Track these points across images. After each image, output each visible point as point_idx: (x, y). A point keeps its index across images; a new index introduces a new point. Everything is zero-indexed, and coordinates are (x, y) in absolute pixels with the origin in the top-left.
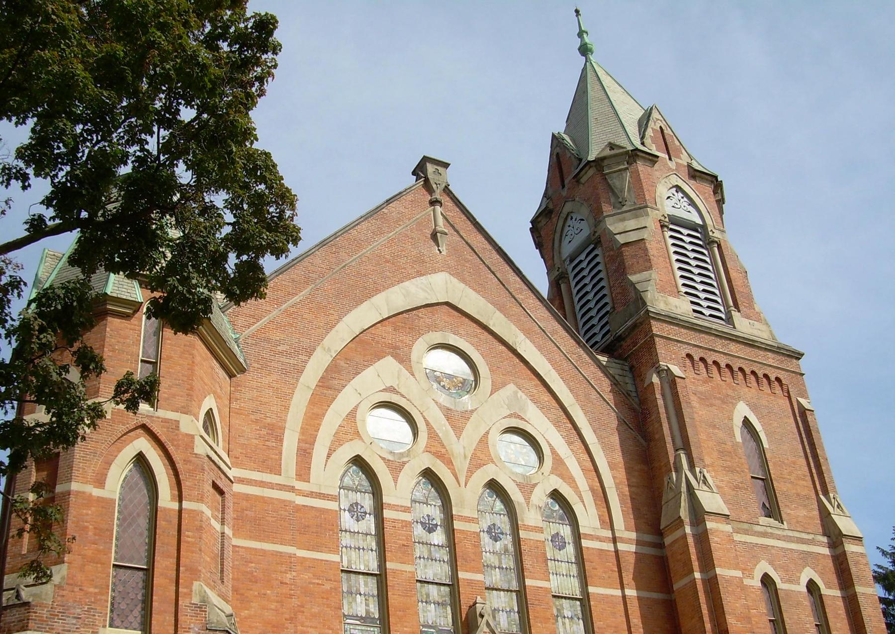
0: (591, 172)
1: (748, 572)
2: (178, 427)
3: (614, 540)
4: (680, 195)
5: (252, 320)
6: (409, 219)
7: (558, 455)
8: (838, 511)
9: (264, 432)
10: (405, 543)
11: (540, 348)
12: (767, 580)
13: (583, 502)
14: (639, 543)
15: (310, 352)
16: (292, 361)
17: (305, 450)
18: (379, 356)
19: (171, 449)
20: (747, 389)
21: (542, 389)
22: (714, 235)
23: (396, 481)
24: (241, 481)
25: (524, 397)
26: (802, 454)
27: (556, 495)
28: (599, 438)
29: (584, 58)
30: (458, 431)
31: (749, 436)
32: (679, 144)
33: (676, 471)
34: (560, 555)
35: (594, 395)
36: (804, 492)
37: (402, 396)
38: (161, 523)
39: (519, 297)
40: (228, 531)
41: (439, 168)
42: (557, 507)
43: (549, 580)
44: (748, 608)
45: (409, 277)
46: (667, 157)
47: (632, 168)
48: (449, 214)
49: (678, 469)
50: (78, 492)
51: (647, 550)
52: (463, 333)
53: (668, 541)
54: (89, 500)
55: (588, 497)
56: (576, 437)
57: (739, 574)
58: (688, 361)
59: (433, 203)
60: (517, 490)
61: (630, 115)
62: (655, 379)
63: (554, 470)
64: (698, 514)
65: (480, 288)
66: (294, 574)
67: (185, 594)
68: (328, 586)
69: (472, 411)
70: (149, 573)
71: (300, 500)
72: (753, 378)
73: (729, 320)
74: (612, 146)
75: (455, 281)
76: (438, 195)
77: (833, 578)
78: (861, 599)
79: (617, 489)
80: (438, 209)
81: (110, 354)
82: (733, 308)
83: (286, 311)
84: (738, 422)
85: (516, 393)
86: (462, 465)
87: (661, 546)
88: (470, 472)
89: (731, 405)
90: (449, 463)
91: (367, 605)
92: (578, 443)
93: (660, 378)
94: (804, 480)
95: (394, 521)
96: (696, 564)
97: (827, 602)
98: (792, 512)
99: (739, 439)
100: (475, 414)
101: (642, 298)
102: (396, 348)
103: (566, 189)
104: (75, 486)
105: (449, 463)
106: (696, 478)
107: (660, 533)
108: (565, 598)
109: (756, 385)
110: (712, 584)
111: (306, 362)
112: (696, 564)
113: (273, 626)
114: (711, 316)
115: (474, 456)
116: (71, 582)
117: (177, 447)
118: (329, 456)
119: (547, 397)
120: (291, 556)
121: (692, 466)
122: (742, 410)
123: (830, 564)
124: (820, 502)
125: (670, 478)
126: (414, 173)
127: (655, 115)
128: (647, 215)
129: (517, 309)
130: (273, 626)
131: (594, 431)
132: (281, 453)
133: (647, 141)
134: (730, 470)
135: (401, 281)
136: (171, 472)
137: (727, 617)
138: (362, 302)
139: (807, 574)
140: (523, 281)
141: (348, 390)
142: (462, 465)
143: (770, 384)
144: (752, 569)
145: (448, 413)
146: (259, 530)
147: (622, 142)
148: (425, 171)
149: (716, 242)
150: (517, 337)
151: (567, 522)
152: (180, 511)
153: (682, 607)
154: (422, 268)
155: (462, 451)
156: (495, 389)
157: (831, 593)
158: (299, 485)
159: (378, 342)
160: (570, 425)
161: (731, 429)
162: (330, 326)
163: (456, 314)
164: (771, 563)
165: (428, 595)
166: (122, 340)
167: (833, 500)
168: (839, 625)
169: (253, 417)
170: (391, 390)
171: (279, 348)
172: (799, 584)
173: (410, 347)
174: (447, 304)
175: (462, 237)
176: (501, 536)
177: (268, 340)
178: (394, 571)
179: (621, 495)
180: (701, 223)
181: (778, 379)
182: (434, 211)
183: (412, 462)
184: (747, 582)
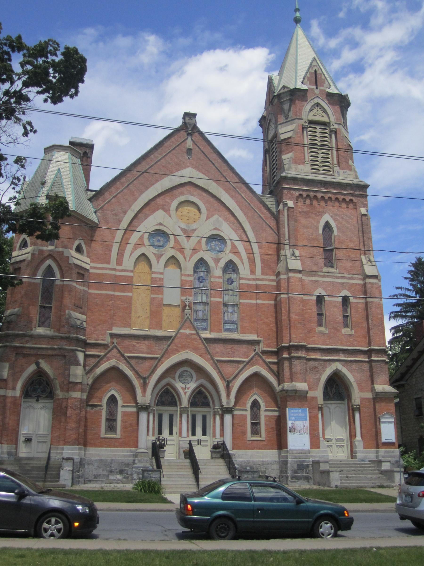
11: (232, 197)
15: (125, 213)
35: (256, 215)
37: (165, 226)
55: (246, 262)
60: (212, 261)
69: (196, 229)
71: (118, 273)
88: (192, 256)
100: (197, 231)
111: (124, 217)
114: (324, 170)
118: (130, 255)
119: (232, 219)
120: (112, 295)
122: (327, 217)
131: (254, 232)
138: (150, 187)
142: (188, 253)
154: (180, 166)
156: (208, 218)
158: (118, 267)
161: (318, 228)
164: (324, 289)
170: (160, 224)
173: (170, 204)
175: (200, 149)
176: (204, 281)
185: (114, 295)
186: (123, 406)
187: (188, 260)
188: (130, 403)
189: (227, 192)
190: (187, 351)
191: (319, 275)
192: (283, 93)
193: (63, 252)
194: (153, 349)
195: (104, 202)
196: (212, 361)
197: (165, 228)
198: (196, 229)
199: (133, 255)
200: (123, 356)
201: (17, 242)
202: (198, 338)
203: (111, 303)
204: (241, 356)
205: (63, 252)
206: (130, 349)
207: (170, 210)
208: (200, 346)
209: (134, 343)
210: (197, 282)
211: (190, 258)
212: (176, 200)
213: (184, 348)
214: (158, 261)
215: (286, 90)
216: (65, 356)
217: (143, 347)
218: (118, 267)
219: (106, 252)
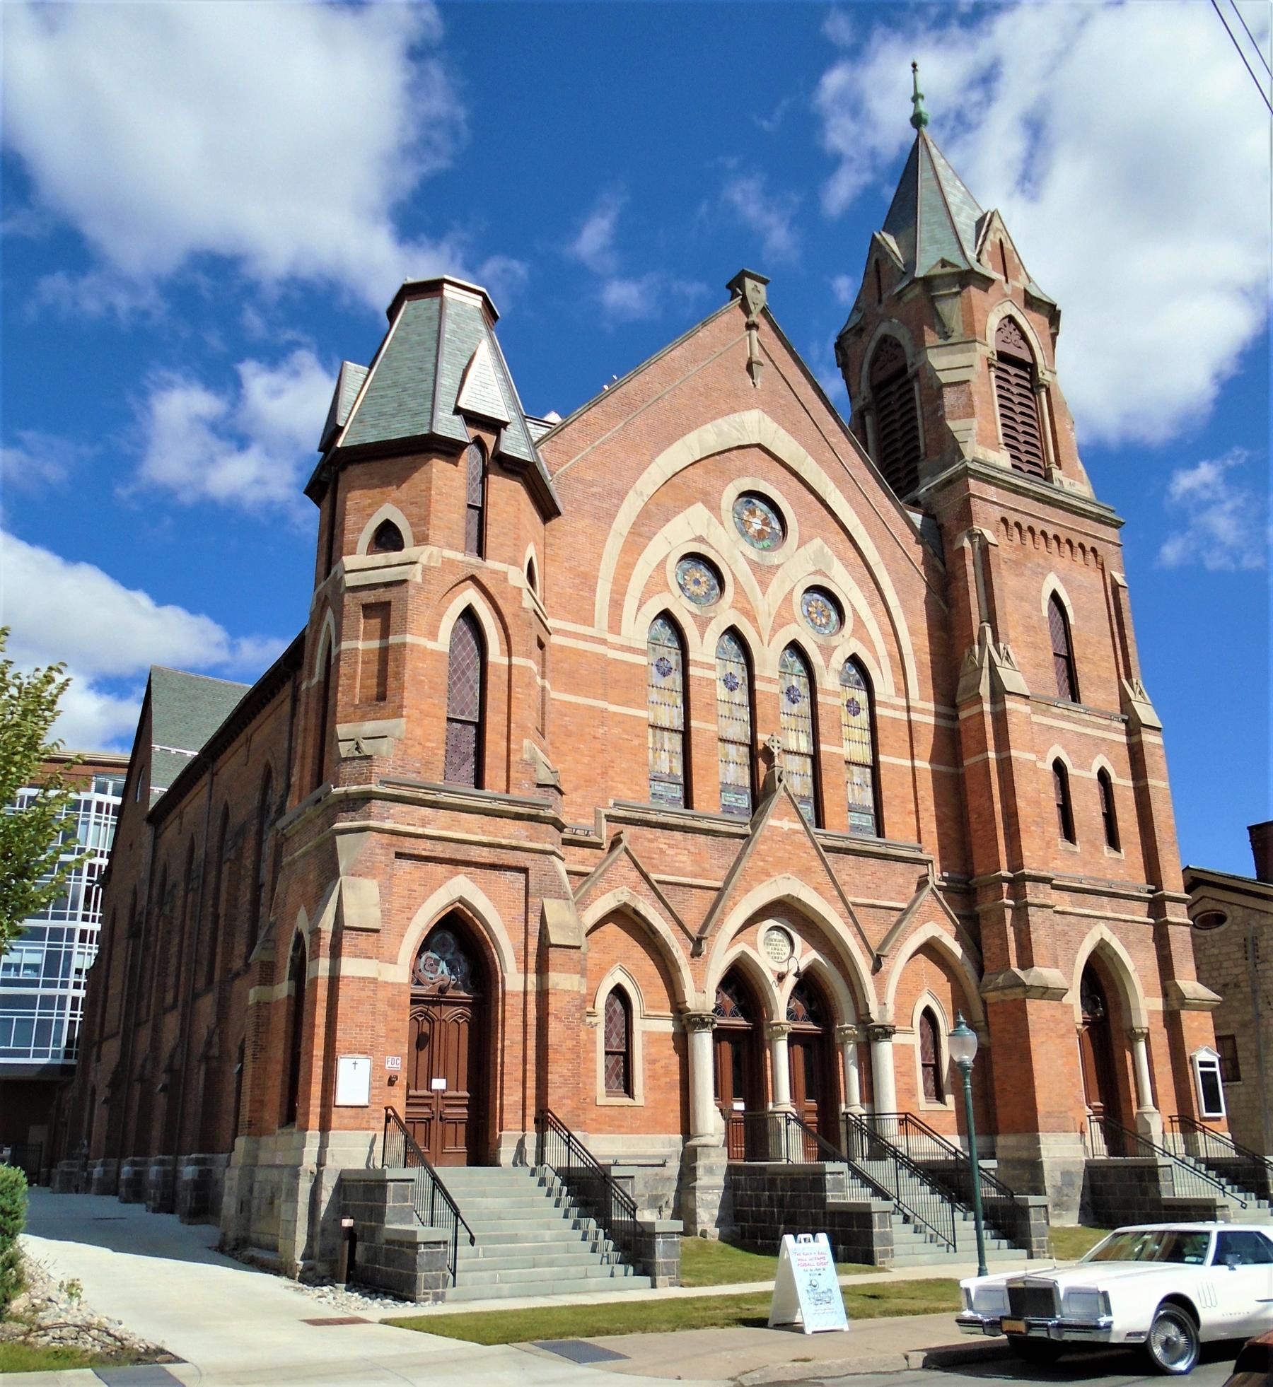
0: (917, 290)
1: (1042, 756)
2: (506, 579)
3: (908, 709)
4: (1013, 326)
5: (566, 458)
6: (724, 345)
7: (859, 617)
8: (1139, 698)
9: (577, 581)
10: (709, 701)
11: (849, 499)
12: (1059, 767)
13: (880, 668)
14: (937, 715)
15: (622, 496)
16: (604, 505)
17: (616, 602)
18: (690, 503)
19: (500, 602)
20: (1060, 559)
21: (849, 544)
22: (1044, 377)
23: (702, 637)
24: (558, 631)
25: (830, 552)
26: (1109, 633)
27: (854, 660)
28: (902, 601)
29: (915, 130)
30: (764, 585)
31: (1056, 609)
32: (1012, 248)
33: (979, 644)
34: (855, 721)
36: (1105, 675)
38: (491, 678)
39: (832, 440)
40: (548, 686)
41: (758, 284)
42: (854, 671)
43: (842, 746)
44: (1039, 792)
45: (722, 414)
46: (1003, 278)
47: (965, 293)
48: (765, 341)
49: (982, 643)
50: (413, 645)
51: (943, 723)
52: (773, 478)
53: (963, 715)
54: (425, 652)
56: (879, 599)
57: (1032, 757)
58: (1002, 527)
59: (751, 326)
60: (817, 651)
61: (965, 222)
62: (966, 543)
63: (854, 633)
64: (998, 692)
65: (793, 431)
66: (606, 728)
67: (517, 750)
68: (636, 742)
69: (778, 566)
70: (480, 727)
72: (1067, 547)
73: (1048, 477)
74: (944, 263)
75: (768, 419)
76: (756, 317)
77: (1127, 769)
78: (1152, 792)
79: (915, 656)
80: (754, 333)
81: (438, 498)
82: (1054, 465)
83: (598, 447)
84: (1046, 595)
85: (822, 548)
86: (766, 622)
87: (955, 718)
88: (774, 631)
89: (1040, 576)
90: (753, 619)
91: (671, 761)
92: (881, 605)
93: (972, 543)
94: (1106, 661)
95: (700, 678)
96: (991, 743)
97: (1116, 791)
98: (1091, 695)
99: (1045, 613)
101: (959, 450)
102: (707, 494)
103: (883, 305)
104: (409, 639)
105: (753, 619)
106: (999, 654)
107: (955, 706)
108: (856, 764)
109: (1069, 554)
110: (1006, 765)
111: (618, 506)
112: (991, 743)
113: (586, 781)
114: (1030, 472)
115: (778, 615)
116: (410, 736)
117: (506, 599)
118: (638, 610)
119: (852, 553)
121: (996, 640)
123: (1125, 752)
124: (1122, 689)
125: (972, 651)
126: (728, 287)
127: (996, 223)
128: (975, 350)
129: (830, 454)
130: (586, 781)
131: (897, 594)
132: (594, 604)
133: (984, 258)
134: (1034, 646)
135: (713, 418)
136: (500, 625)
137: (1018, 800)
139: (1100, 761)
140: (837, 421)
141: (658, 538)
142: (766, 622)
143: (1084, 555)
144: (1046, 752)
145: (755, 566)
146: (574, 684)
147: (955, 258)
148: (743, 288)
149: (1045, 386)
150: (827, 486)
151: (863, 687)
152: (510, 666)
153: (971, 784)
154: (734, 403)
155: (767, 608)
156: (802, 543)
157: (1123, 783)
158: (611, 638)
159: (688, 486)
160: (873, 586)
162: (641, 468)
163: (767, 456)
164: (1064, 747)
165: (727, 755)
166: (447, 482)
167: (1135, 686)
168: (1126, 816)
169: (566, 564)
170: (700, 539)
171: (592, 489)
172: (1090, 771)
173: (721, 493)
174: (759, 446)
177: (581, 481)
178: (698, 730)
179: (919, 666)
180: (1031, 362)
181: (1094, 550)
182: (750, 335)
183: (718, 617)
184: (1039, 765)
185: (604, 711)
186: (648, 1017)
187: (766, 643)
188: (661, 1008)
189: (837, 487)
190: (788, 875)
191: (1053, 713)
192: (941, 276)
193: (506, 573)
194: (707, 866)
195: (571, 458)
196: (841, 905)
197: (713, 551)
198: (778, 566)
199: (643, 609)
200: (645, 877)
201: (360, 530)
202: (809, 844)
203: (601, 731)
204: (893, 895)
205: (506, 573)
206: (655, 861)
207: (720, 509)
208: (815, 864)
209: (662, 846)
210: (784, 698)
211: (771, 637)
212: (731, 484)
213: (782, 865)
214: (702, 635)
215: (948, 270)
216: (525, 870)
217: (684, 858)
218: (611, 638)
219: (581, 593)
